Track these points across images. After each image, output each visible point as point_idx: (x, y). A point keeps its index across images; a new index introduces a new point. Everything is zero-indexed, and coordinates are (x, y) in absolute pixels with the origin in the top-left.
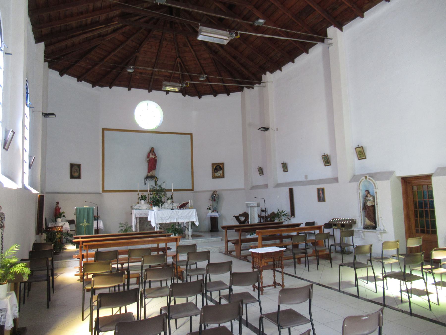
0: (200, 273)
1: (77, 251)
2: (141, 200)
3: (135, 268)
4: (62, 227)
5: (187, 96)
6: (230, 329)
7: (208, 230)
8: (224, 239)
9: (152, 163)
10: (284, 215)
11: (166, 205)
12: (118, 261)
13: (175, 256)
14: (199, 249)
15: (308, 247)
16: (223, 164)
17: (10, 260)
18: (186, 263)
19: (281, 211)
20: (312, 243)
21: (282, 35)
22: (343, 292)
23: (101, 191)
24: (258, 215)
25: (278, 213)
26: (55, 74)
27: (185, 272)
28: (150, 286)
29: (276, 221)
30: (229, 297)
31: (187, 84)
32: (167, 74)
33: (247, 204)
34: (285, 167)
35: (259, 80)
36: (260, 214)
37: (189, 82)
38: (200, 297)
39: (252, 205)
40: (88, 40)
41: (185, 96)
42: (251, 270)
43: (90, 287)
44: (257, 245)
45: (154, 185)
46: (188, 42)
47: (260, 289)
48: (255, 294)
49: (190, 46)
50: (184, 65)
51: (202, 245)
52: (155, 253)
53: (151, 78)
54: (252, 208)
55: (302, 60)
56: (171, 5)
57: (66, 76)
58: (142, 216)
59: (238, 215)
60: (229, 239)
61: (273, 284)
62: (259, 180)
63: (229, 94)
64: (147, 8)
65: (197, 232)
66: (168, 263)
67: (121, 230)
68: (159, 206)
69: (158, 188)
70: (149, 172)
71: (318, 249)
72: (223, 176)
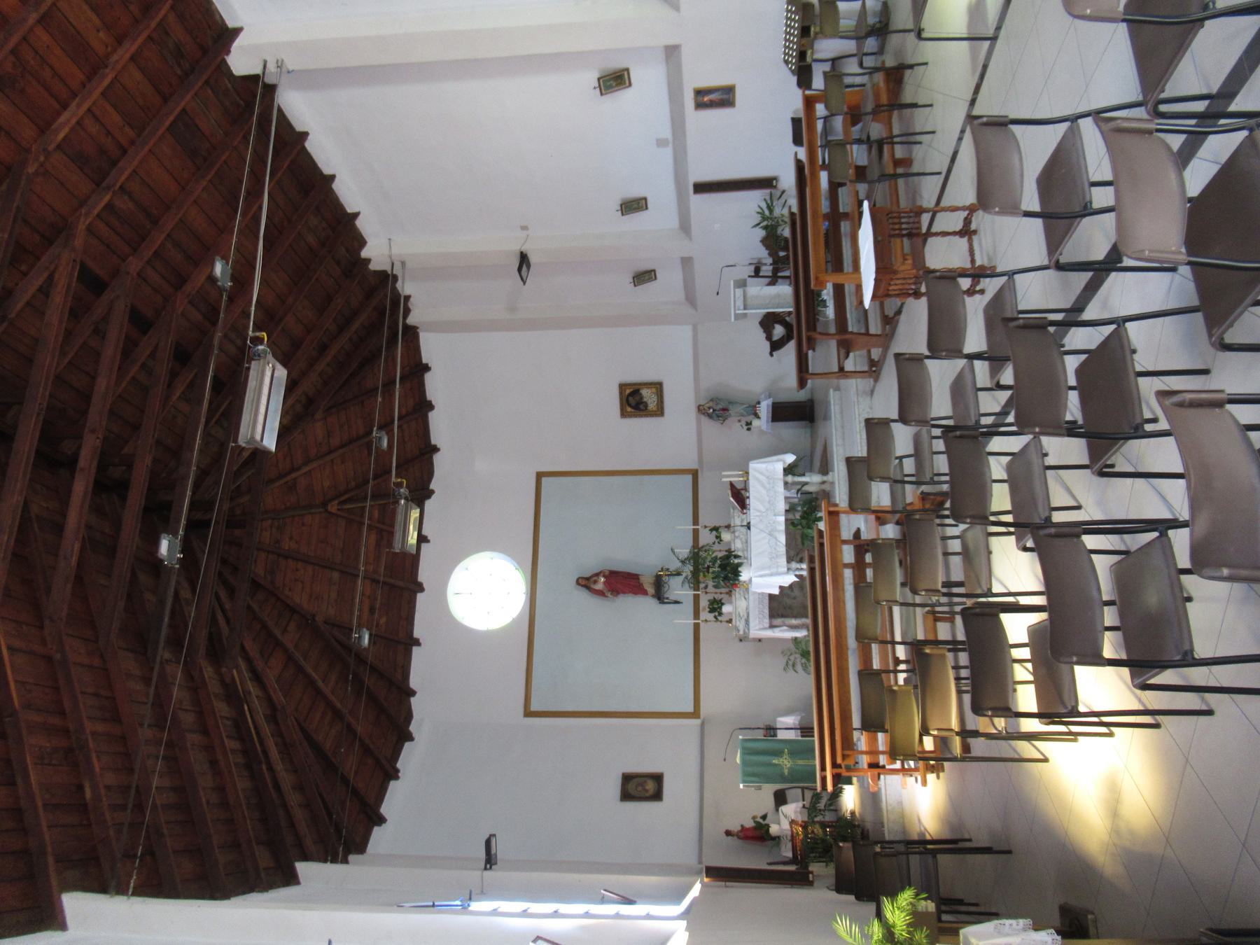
0: (926, 445)
1: (860, 780)
2: (720, 614)
3: (908, 623)
4: (792, 822)
5: (432, 487)
6: (1084, 357)
7: (808, 430)
8: (835, 381)
9: (620, 583)
10: (770, 208)
11: (737, 546)
12: (888, 672)
13: (878, 518)
14: (860, 449)
15: (864, 137)
16: (622, 387)
17: (875, 938)
18: (899, 485)
19: (758, 218)
20: (854, 124)
21: (254, 209)
22: (998, 28)
23: (697, 722)
24: (770, 284)
25: (765, 228)
26: (379, 836)
27: (924, 488)
28: (960, 584)
29: (787, 233)
30: (995, 359)
31: (399, 485)
32: (373, 537)
33: (737, 317)
34: (633, 206)
35: (386, 279)
36: (768, 280)
37: (393, 479)
38: (996, 444)
39: (740, 303)
40: (286, 748)
41: (432, 492)
42: (924, 300)
43: (957, 740)
44: (853, 288)
45: (680, 579)
46: (282, 481)
47: (978, 274)
48: (991, 286)
49: (293, 475)
50: (347, 491)
51: (846, 439)
52: (869, 573)
53: (384, 583)
54: (749, 302)
55: (325, 151)
56: (183, 522)
57: (384, 810)
58: (767, 611)
59: (767, 344)
60: (836, 369)
61: (965, 239)
62: (669, 282)
63: (427, 368)
64: (194, 591)
65: (812, 459)
66: (898, 537)
67: (805, 668)
68: (740, 565)
69: (688, 569)
70: (645, 593)
71: (869, 107)
72: (658, 387)
